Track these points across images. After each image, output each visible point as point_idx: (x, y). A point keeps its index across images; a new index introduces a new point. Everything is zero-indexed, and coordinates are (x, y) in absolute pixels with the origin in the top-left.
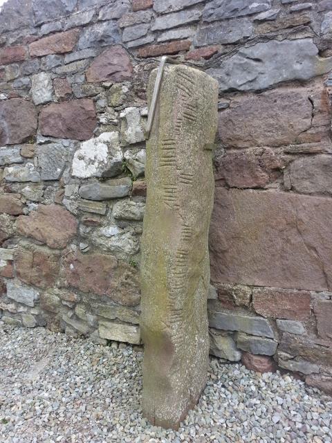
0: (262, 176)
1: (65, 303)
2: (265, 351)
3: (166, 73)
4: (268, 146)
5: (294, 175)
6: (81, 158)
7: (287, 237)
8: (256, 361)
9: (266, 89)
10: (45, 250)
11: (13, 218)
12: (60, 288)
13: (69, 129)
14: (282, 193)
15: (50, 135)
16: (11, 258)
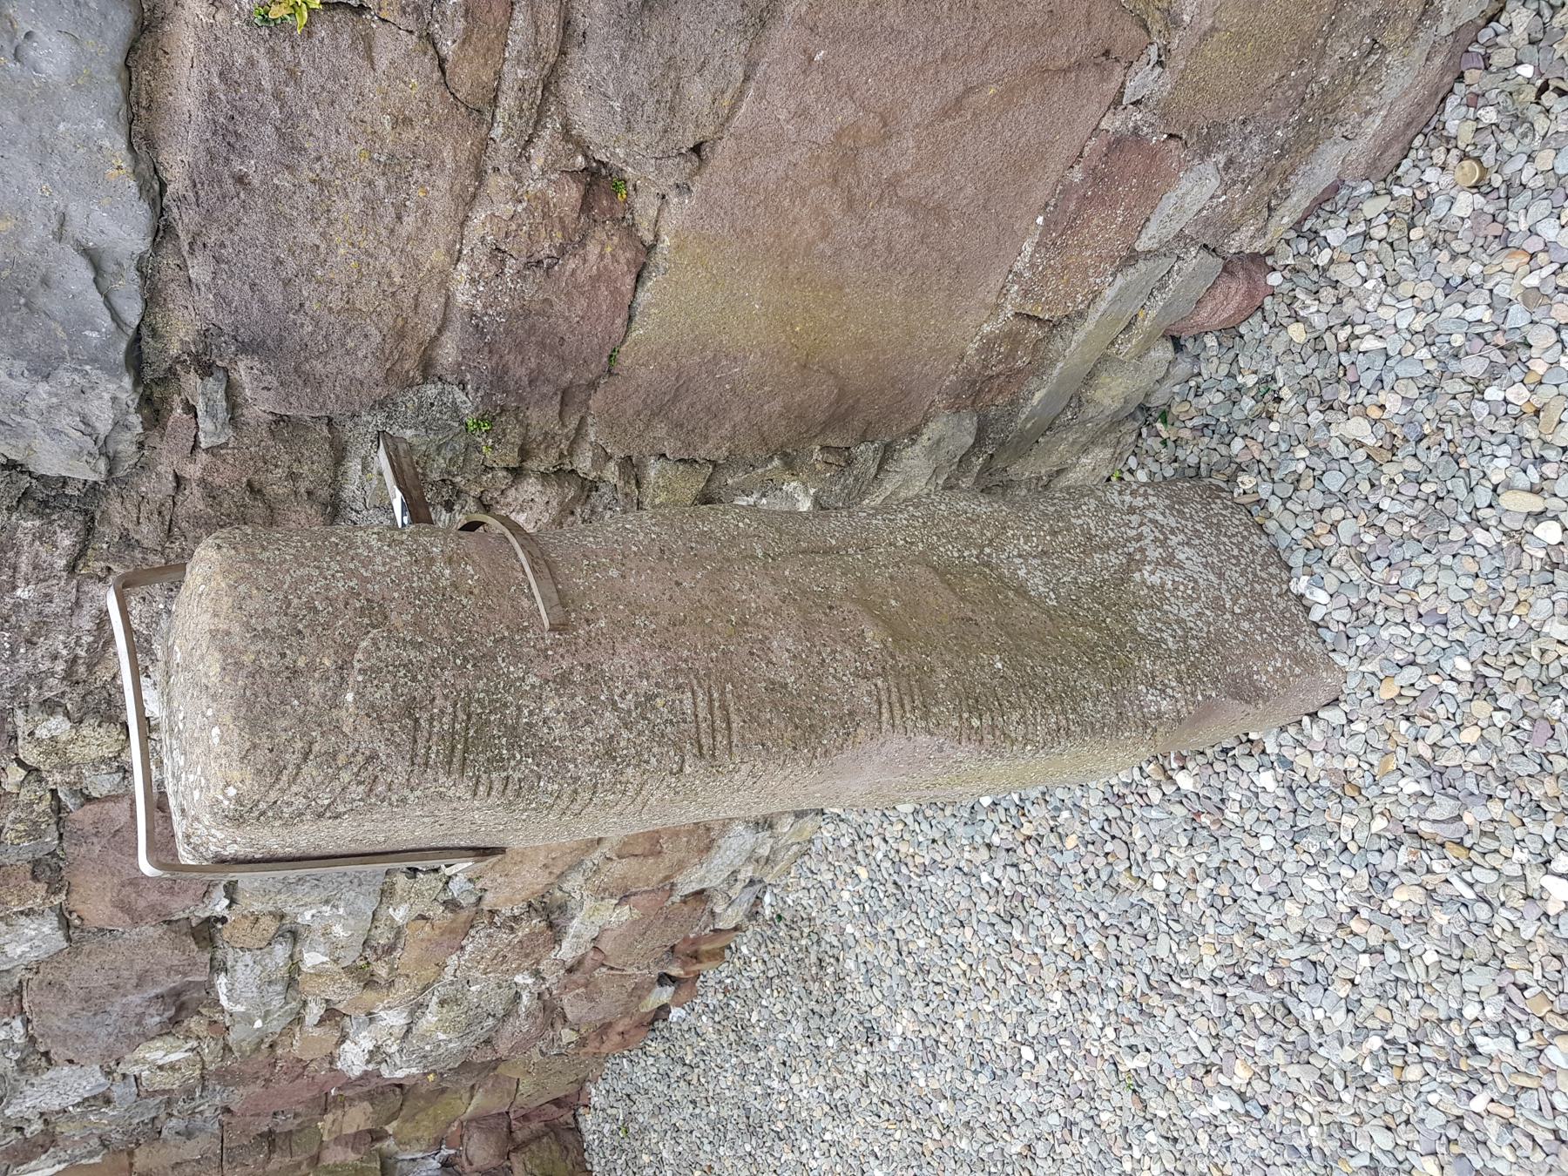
0: (602, 256)
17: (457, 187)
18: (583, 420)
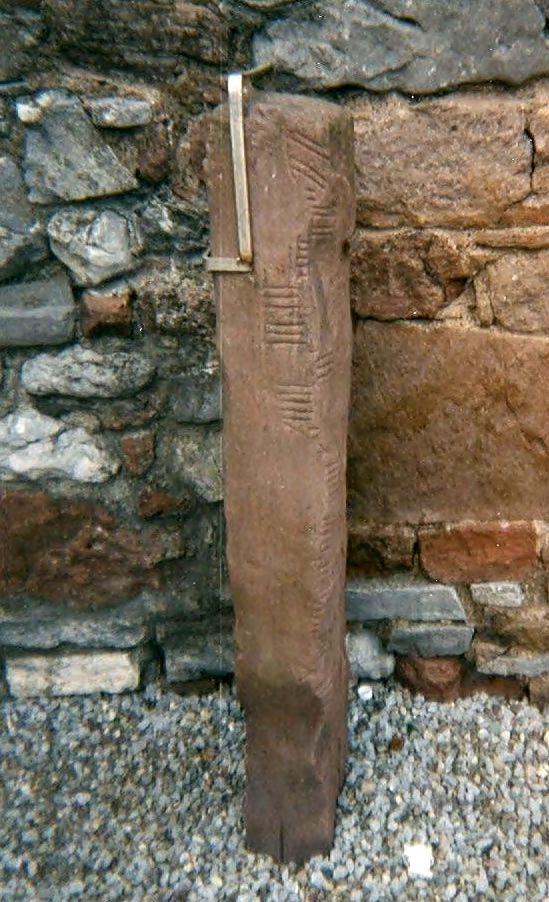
4: (440, 227)
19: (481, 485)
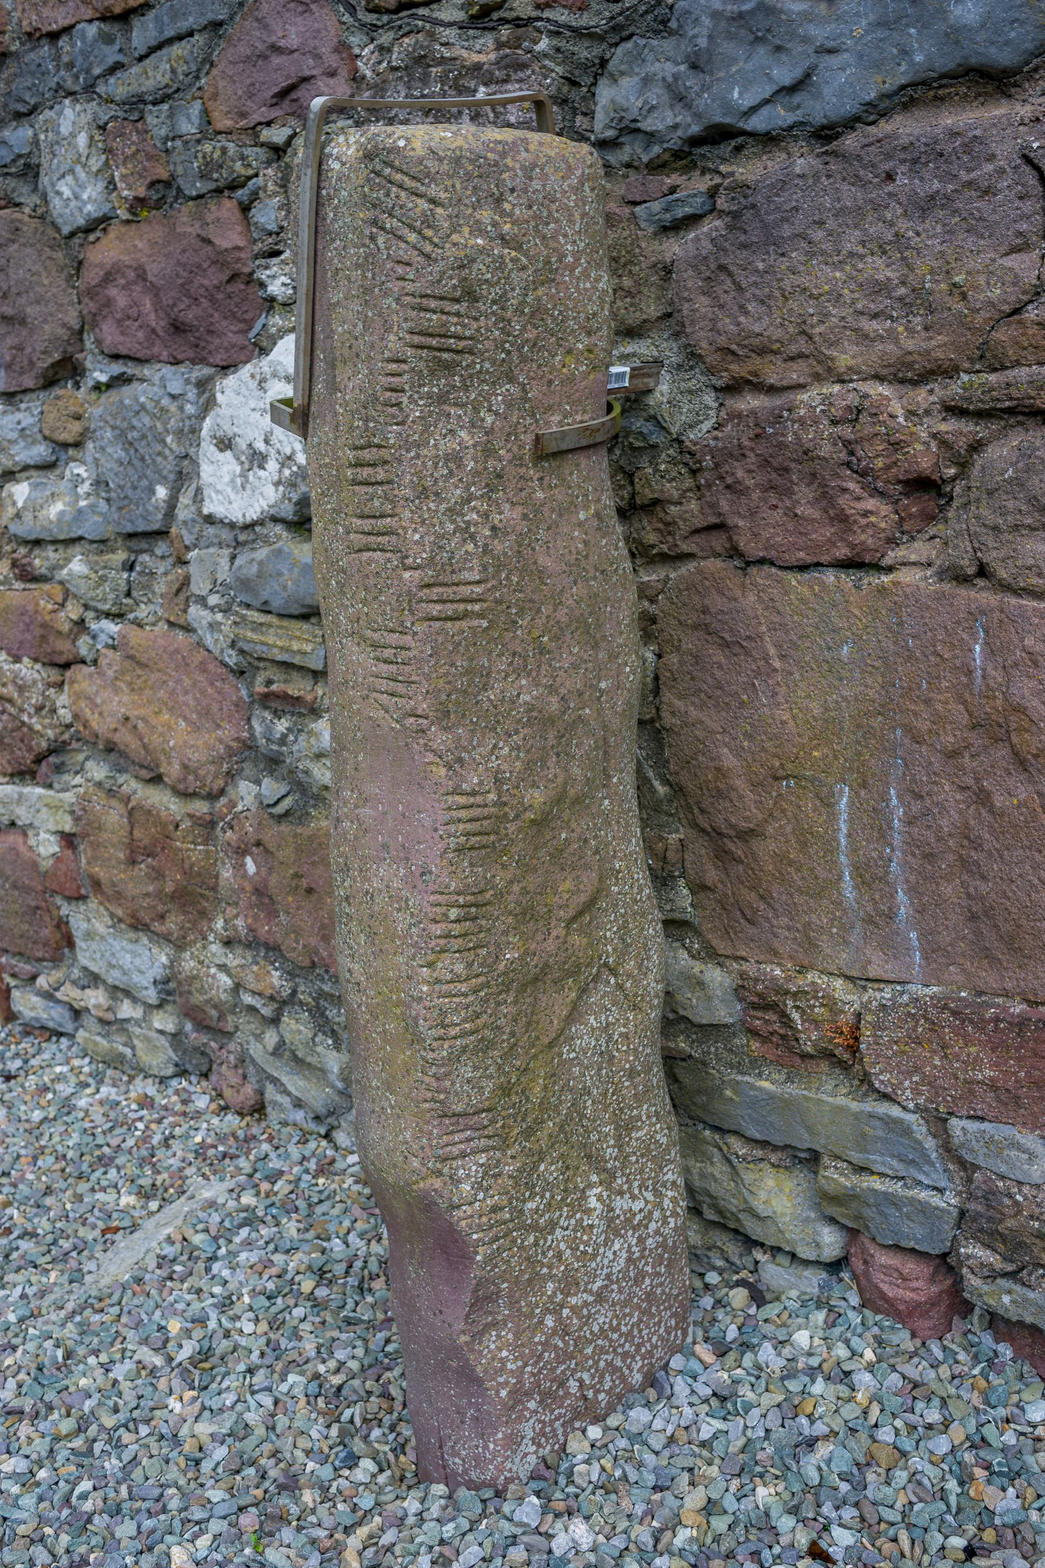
0: (866, 514)
1: (248, 999)
2: (915, 1234)
3: (336, 166)
4: (879, 378)
5: (984, 512)
6: (225, 444)
7: (977, 780)
8: (886, 1270)
9: (851, 123)
10: (162, 801)
11: (54, 675)
12: (228, 943)
13: (178, 328)
14: (947, 587)
15: (124, 352)
16: (68, 826)
17: (910, 358)
18: (691, 556)
19: (973, 917)
